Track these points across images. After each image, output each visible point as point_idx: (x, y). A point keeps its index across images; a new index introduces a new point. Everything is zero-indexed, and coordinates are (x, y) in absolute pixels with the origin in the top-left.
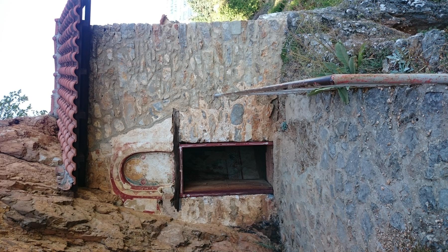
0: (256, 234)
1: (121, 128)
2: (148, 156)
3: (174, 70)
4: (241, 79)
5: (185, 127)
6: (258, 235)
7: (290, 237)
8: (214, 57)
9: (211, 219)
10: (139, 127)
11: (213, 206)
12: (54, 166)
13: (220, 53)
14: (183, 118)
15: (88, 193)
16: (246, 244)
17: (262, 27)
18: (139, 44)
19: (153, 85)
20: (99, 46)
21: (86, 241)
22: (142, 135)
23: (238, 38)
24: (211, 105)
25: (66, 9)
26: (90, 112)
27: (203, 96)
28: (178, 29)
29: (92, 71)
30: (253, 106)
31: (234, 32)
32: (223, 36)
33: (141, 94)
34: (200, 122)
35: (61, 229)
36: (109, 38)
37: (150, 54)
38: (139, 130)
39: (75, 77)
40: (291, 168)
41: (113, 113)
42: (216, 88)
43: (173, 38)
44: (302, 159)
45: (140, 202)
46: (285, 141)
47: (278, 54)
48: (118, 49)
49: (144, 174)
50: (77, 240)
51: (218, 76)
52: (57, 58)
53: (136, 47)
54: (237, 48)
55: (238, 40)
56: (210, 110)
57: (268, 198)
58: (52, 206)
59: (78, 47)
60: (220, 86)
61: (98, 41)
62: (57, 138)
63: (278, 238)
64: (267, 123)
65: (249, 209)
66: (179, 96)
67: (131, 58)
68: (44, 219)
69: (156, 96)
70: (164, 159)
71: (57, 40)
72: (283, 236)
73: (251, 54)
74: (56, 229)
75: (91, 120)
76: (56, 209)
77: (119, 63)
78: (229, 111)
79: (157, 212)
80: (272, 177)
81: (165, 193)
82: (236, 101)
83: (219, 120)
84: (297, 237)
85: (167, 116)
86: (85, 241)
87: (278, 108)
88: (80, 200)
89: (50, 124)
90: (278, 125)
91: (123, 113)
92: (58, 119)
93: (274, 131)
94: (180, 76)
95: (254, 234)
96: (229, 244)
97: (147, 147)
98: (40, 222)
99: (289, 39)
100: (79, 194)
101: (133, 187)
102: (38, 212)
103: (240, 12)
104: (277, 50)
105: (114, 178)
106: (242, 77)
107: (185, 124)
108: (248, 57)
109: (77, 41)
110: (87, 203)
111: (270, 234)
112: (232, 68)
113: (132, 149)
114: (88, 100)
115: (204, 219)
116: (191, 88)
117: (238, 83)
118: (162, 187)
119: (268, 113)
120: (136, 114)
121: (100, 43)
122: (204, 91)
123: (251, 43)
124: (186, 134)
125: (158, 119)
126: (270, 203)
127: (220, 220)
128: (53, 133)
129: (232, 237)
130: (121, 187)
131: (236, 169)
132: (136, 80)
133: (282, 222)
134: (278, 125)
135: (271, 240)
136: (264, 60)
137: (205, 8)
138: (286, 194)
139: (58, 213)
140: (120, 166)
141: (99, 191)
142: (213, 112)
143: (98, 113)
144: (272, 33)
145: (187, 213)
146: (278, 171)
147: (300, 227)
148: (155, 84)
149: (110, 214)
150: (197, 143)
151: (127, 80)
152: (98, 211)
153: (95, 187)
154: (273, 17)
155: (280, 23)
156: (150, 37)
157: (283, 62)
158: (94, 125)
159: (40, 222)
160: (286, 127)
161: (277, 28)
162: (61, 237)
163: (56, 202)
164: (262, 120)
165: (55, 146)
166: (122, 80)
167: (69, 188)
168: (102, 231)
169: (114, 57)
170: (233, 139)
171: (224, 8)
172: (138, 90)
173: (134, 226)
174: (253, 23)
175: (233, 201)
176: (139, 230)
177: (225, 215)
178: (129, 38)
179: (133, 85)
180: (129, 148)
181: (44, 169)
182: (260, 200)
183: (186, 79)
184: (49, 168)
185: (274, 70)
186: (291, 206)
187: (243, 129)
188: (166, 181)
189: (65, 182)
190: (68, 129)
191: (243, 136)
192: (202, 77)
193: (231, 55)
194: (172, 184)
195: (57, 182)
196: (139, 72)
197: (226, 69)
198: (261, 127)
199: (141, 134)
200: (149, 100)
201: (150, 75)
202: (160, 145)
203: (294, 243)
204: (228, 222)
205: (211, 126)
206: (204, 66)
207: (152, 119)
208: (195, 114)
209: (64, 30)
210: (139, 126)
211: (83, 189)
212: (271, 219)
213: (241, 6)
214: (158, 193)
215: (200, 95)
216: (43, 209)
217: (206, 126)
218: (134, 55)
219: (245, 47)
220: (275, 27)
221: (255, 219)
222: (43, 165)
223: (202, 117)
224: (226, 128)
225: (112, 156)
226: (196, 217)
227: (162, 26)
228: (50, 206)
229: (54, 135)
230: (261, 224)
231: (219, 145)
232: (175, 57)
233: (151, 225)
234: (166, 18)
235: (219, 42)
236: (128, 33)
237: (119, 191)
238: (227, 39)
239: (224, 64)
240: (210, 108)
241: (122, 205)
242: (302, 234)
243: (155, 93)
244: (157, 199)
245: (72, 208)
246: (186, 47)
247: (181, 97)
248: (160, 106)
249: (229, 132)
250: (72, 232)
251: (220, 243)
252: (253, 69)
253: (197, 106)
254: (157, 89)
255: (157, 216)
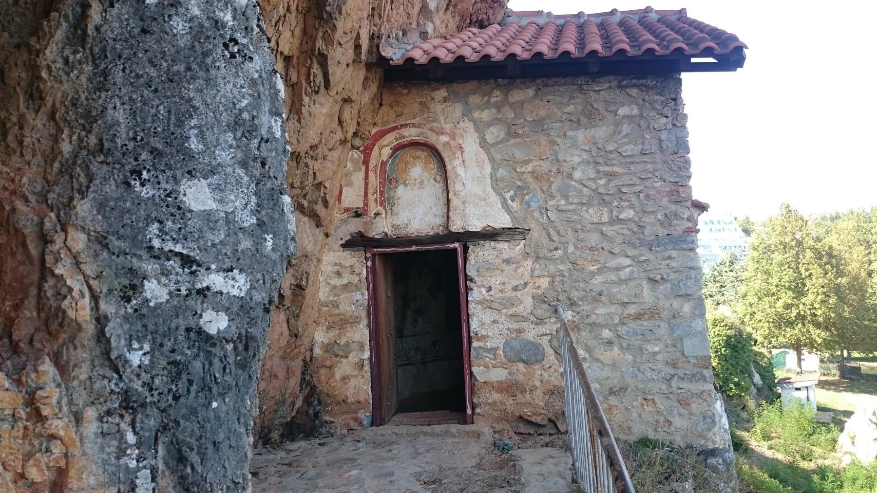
0: (298, 393)
1: (490, 138)
2: (439, 187)
3: (604, 229)
4: (594, 358)
5: (495, 253)
6: (297, 397)
7: (296, 458)
8: (634, 303)
9: (327, 306)
10: (493, 168)
11: (349, 309)
12: (418, 24)
13: (643, 315)
14: (512, 247)
15: (374, 88)
16: (281, 375)
17: (701, 399)
18: (651, 163)
19: (572, 189)
20: (643, 91)
21: (293, 88)
22: (478, 174)
23: (675, 351)
24: (540, 299)
25: (708, 28)
26: (518, 81)
27: (556, 284)
28: (685, 234)
29: (593, 81)
30: (542, 381)
31: (688, 343)
32: (678, 321)
33: (554, 170)
34: (505, 280)
35: (314, 44)
36: (659, 107)
37: (632, 183)
38: (488, 169)
39: (583, 52)
40: (425, 460)
41: (518, 122)
42: (574, 308)
43: (666, 224)
44: (445, 481)
45: (358, 178)
46: (475, 448)
47: (649, 433)
48: (639, 126)
49: (407, 182)
50: (296, 73)
51: (597, 312)
52: (614, 17)
53: (645, 156)
54: (656, 349)
55: (671, 350)
56: (530, 299)
57: (365, 415)
58: (353, 26)
59: (640, 53)
60: (577, 317)
61: (652, 88)
62: (466, 27)
63: (290, 437)
64: (509, 412)
65: (345, 379)
66: (554, 238)
67: (624, 149)
68: (333, 15)
69: (552, 197)
70: (435, 216)
71: (646, 14)
72: (295, 446)
73: (645, 378)
74: (314, 35)
75: (504, 85)
76: (349, 34)
77: (612, 127)
78: (530, 334)
79: (339, 210)
80: (404, 423)
81: (374, 221)
82: (550, 348)
83: (511, 315)
84: (297, 472)
85: (516, 218)
86: (293, 86)
87: (541, 434)
88: (362, 73)
89: (490, 12)
90: (506, 435)
91: (519, 140)
92: (500, 24)
93: (493, 425)
94: (594, 239)
95: (299, 389)
96: (283, 343)
97: (456, 185)
98: (328, 8)
99: (681, 452)
100: (373, 71)
101: (384, 164)
102: (344, 4)
103: (719, 360)
104: (656, 430)
105: (400, 131)
106: (598, 360)
107: (501, 251)
108: (639, 371)
109: (650, 51)
110: (358, 86)
111: (299, 421)
112: (616, 341)
113: (452, 159)
114: (540, 77)
115: (326, 294)
116: (572, 260)
117: (587, 351)
118: (384, 215)
119: (529, 413)
120: (518, 162)
121: (648, 91)
122: (567, 287)
123: (668, 377)
124: (481, 253)
125: (510, 202)
126: (356, 419)
127: (325, 324)
128: (474, 19)
129: (296, 348)
130: (385, 143)
131: (413, 352)
132: (580, 160)
133: (320, 444)
134: (506, 435)
135: (287, 422)
136: (635, 404)
137: (721, 288)
138: (375, 451)
139: (341, 37)
140: (421, 139)
141: (378, 106)
142: (526, 304)
143: (517, 96)
144: (690, 419)
145: (338, 262)
146: (416, 436)
147: (316, 478)
148: (575, 193)
149: (339, 127)
150: (466, 275)
151: (580, 142)
152: (344, 106)
153: (383, 98)
154: (720, 421)
155: (710, 435)
156: (665, 181)
157: (635, 442)
158: (495, 90)
159: (328, 8)
160: (503, 449)
161: (699, 429)
162: (301, 44)
163: (361, 32)
164: (515, 402)
165: (452, 25)
166: (581, 135)
167: (383, 54)
168: (310, 114)
169: (622, 119)
170: (475, 344)
171: (726, 326)
172: (563, 164)
173: (319, 170)
174: (708, 379)
175: (358, 348)
176: (311, 178)
177: (333, 333)
178: (660, 144)
179: (572, 155)
180: (455, 154)
181: (413, 7)
182: (362, 399)
183: (588, 251)
184: (414, 16)
185: (616, 425)
186: (353, 460)
187: (495, 362)
188: (396, 222)
189: (393, 45)
190: (486, 46)
191: (482, 363)
192: (594, 281)
193: (640, 337)
194: (389, 233)
195: (391, 32)
196: (597, 163)
197: (613, 328)
198: (501, 398)
199: (481, 173)
200: (544, 183)
201: (592, 184)
202: (461, 207)
203: (285, 467)
204: (322, 339)
205: (498, 301)
206: (615, 285)
207: (509, 191)
208: (521, 269)
209: (667, 26)
210: (494, 169)
211: (380, 77)
212: (326, 422)
213: (730, 362)
214: (373, 208)
215: (558, 279)
216: (349, 13)
217: (499, 291)
218: (629, 153)
219: (659, 366)
220: (702, 424)
221: (325, 391)
222: (420, 5)
223: (515, 283)
224: (496, 329)
225: (439, 125)
226: (331, 279)
227: (689, 204)
228: (354, 24)
229: (471, 20)
230: (316, 403)
231: (464, 317)
232: (629, 230)
233: (320, 199)
234: (703, 212)
235: (665, 314)
236: (670, 141)
237: (377, 140)
238: (672, 329)
239: (622, 323)
240: (533, 298)
241: (353, 147)
242: (303, 482)
243: (559, 195)
244: (363, 208)
245: (350, 61)
246: (651, 250)
247: (552, 243)
248: (533, 204)
249: (488, 337)
250: (309, 62)
251: (285, 325)
252: (616, 381)
253: (536, 273)
254: (566, 198)
255: (334, 210)
